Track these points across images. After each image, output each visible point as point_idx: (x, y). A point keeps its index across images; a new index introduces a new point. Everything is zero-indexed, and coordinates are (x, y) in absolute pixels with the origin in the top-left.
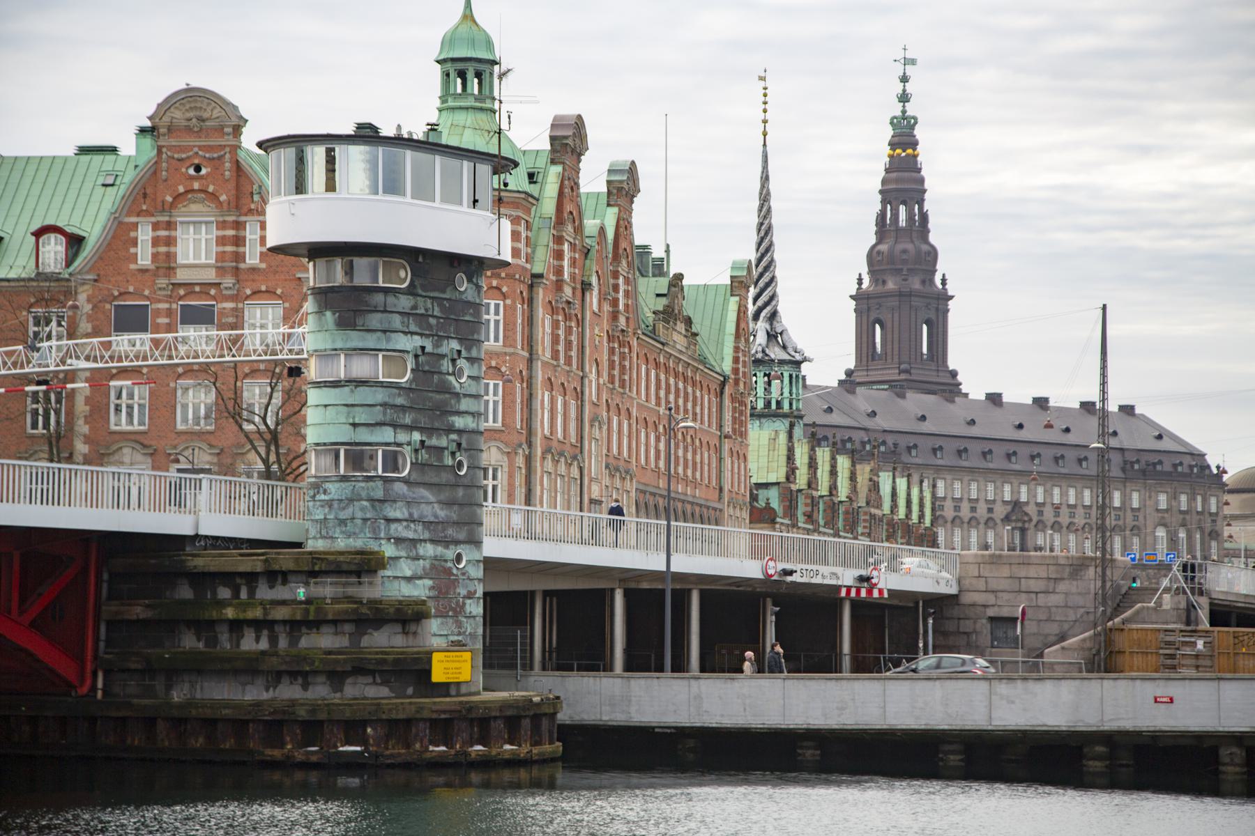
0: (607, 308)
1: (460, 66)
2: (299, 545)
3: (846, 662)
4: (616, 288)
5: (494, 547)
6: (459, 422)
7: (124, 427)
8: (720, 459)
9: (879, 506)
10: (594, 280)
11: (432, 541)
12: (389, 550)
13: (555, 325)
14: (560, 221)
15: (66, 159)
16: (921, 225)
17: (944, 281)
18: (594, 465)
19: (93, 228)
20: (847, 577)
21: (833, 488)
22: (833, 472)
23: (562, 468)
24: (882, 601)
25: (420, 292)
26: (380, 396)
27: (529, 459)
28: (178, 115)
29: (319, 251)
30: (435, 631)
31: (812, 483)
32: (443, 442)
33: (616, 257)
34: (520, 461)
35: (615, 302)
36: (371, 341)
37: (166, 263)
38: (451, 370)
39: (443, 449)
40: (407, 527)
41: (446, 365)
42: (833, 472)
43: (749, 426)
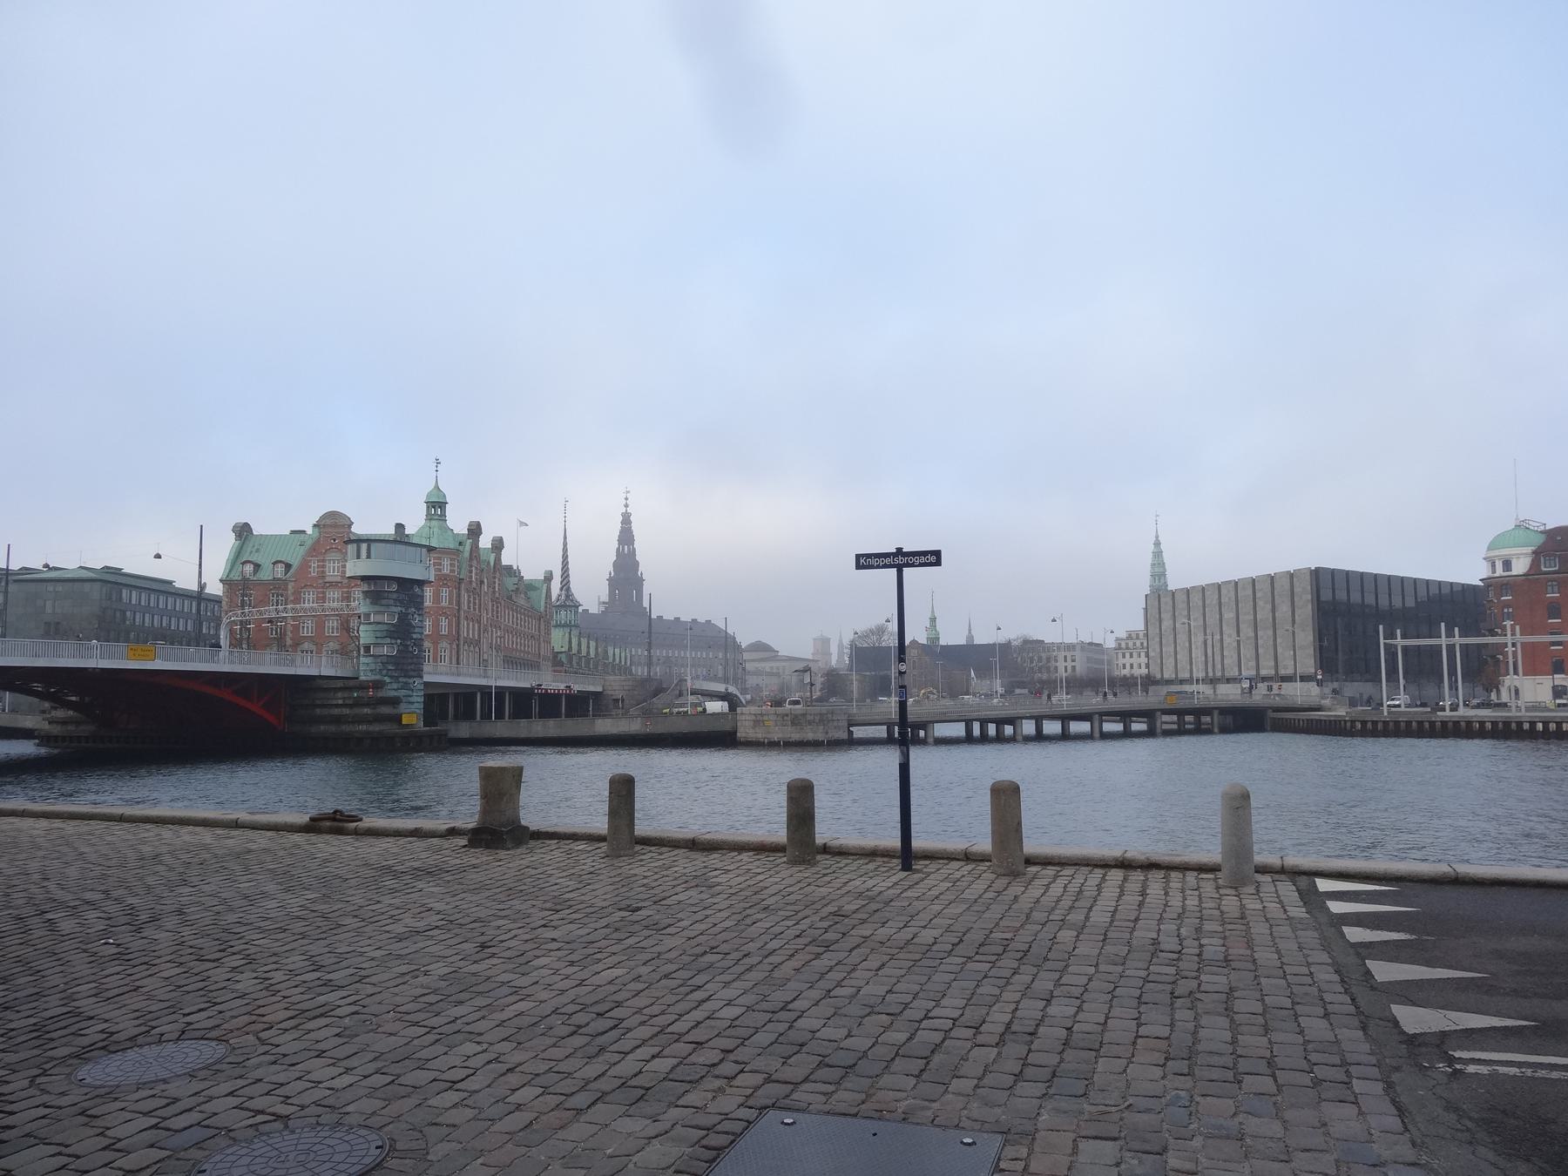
0: (491, 590)
1: (434, 504)
2: (357, 678)
4: (495, 582)
5: (427, 678)
6: (415, 636)
7: (305, 635)
8: (539, 644)
9: (607, 659)
10: (486, 580)
12: (387, 679)
13: (469, 597)
14: (471, 559)
15: (286, 535)
16: (633, 553)
17: (642, 574)
18: (485, 647)
19: (295, 563)
20: (562, 686)
21: (588, 653)
22: (588, 647)
23: (472, 648)
26: (385, 627)
27: (458, 646)
28: (328, 522)
29: (364, 579)
30: (403, 707)
31: (579, 651)
32: (409, 643)
33: (495, 572)
34: (454, 646)
35: (494, 588)
36: (382, 609)
37: (322, 575)
41: (410, 617)
42: (588, 647)
43: (552, 631)
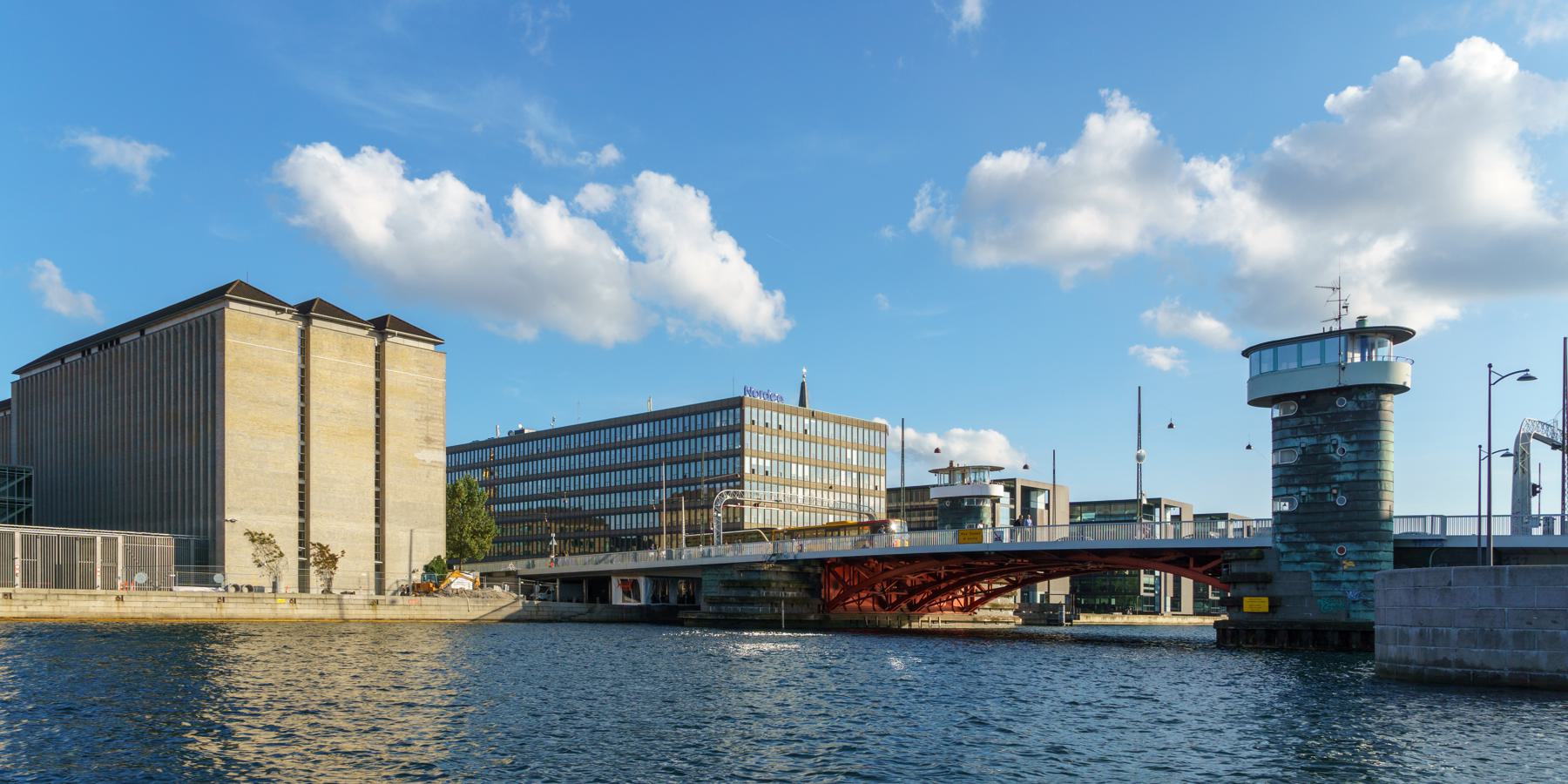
3: (39, 583)
11: (1317, 542)
24: (1177, 569)
25: (1306, 414)
38: (1332, 451)
39: (1326, 493)
40: (1297, 537)
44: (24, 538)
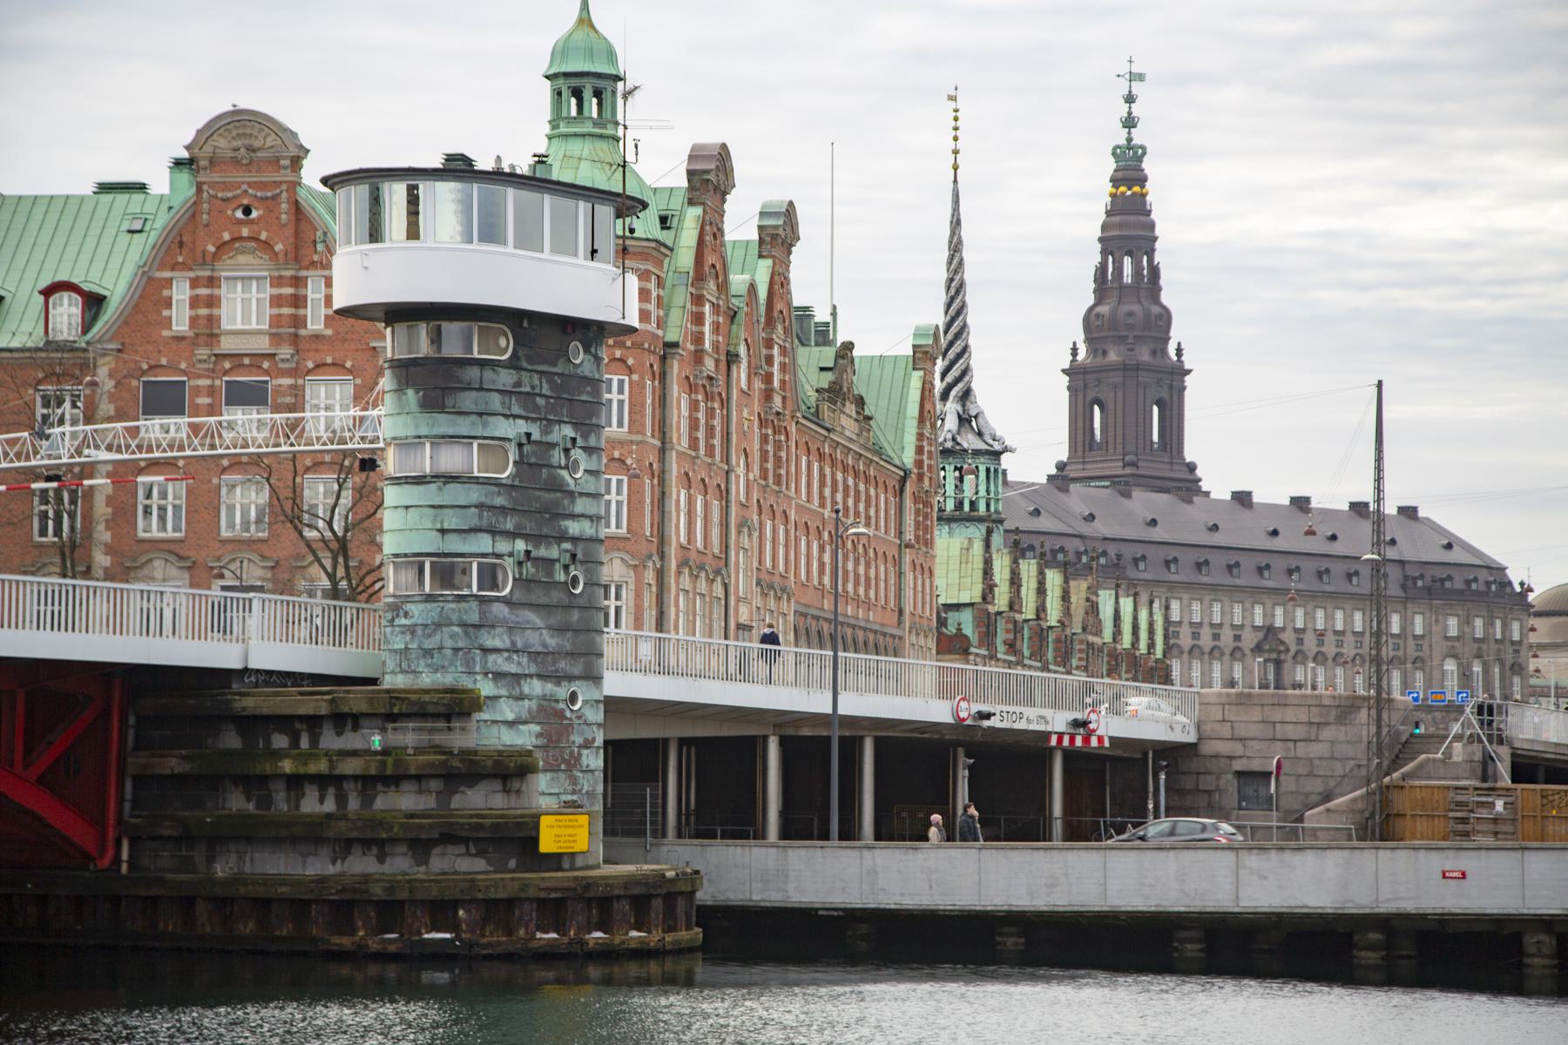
0: (758, 384)
1: (575, 82)
2: (373, 681)
3: (1058, 827)
4: (769, 360)
5: (617, 684)
6: (574, 528)
7: (155, 533)
8: (900, 574)
9: (1098, 633)
10: (742, 350)
11: (540, 676)
12: (486, 688)
13: (694, 406)
14: (699, 277)
15: (82, 199)
16: (1150, 281)
17: (1179, 352)
18: (742, 582)
19: (116, 285)
20: (1058, 721)
21: (1041, 610)
22: (1041, 590)
23: (702, 585)
24: (1101, 752)
25: (525, 365)
26: (474, 495)
27: (661, 574)
28: (222, 144)
29: (399, 314)
30: (543, 789)
31: (1014, 604)
32: (554, 553)
33: (770, 322)
34: (650, 576)
35: (768, 378)
36: (463, 426)
37: (207, 329)
38: (563, 463)
39: (553, 561)
40: (509, 659)
41: (557, 457)
42: (1041, 590)
43: (936, 533)
44: (250, 324)
